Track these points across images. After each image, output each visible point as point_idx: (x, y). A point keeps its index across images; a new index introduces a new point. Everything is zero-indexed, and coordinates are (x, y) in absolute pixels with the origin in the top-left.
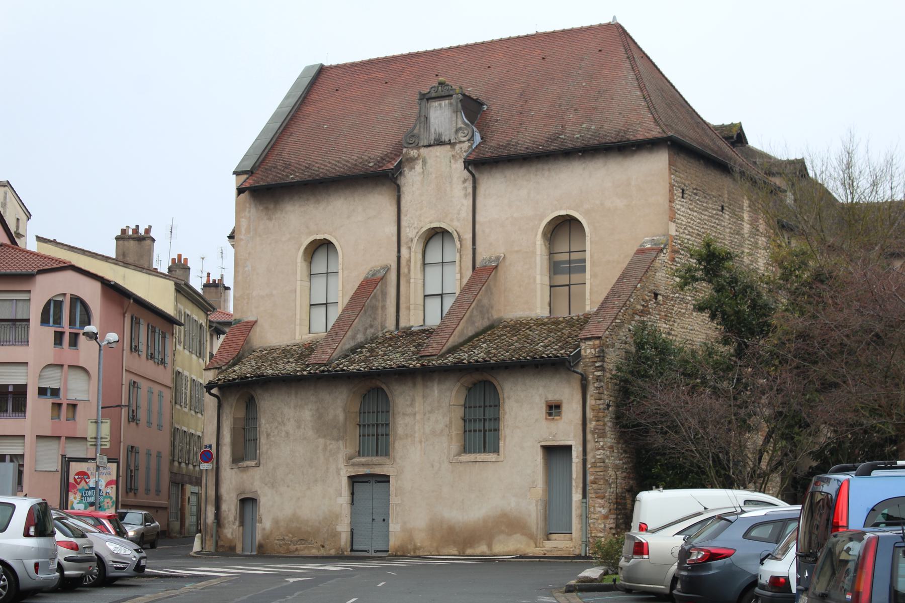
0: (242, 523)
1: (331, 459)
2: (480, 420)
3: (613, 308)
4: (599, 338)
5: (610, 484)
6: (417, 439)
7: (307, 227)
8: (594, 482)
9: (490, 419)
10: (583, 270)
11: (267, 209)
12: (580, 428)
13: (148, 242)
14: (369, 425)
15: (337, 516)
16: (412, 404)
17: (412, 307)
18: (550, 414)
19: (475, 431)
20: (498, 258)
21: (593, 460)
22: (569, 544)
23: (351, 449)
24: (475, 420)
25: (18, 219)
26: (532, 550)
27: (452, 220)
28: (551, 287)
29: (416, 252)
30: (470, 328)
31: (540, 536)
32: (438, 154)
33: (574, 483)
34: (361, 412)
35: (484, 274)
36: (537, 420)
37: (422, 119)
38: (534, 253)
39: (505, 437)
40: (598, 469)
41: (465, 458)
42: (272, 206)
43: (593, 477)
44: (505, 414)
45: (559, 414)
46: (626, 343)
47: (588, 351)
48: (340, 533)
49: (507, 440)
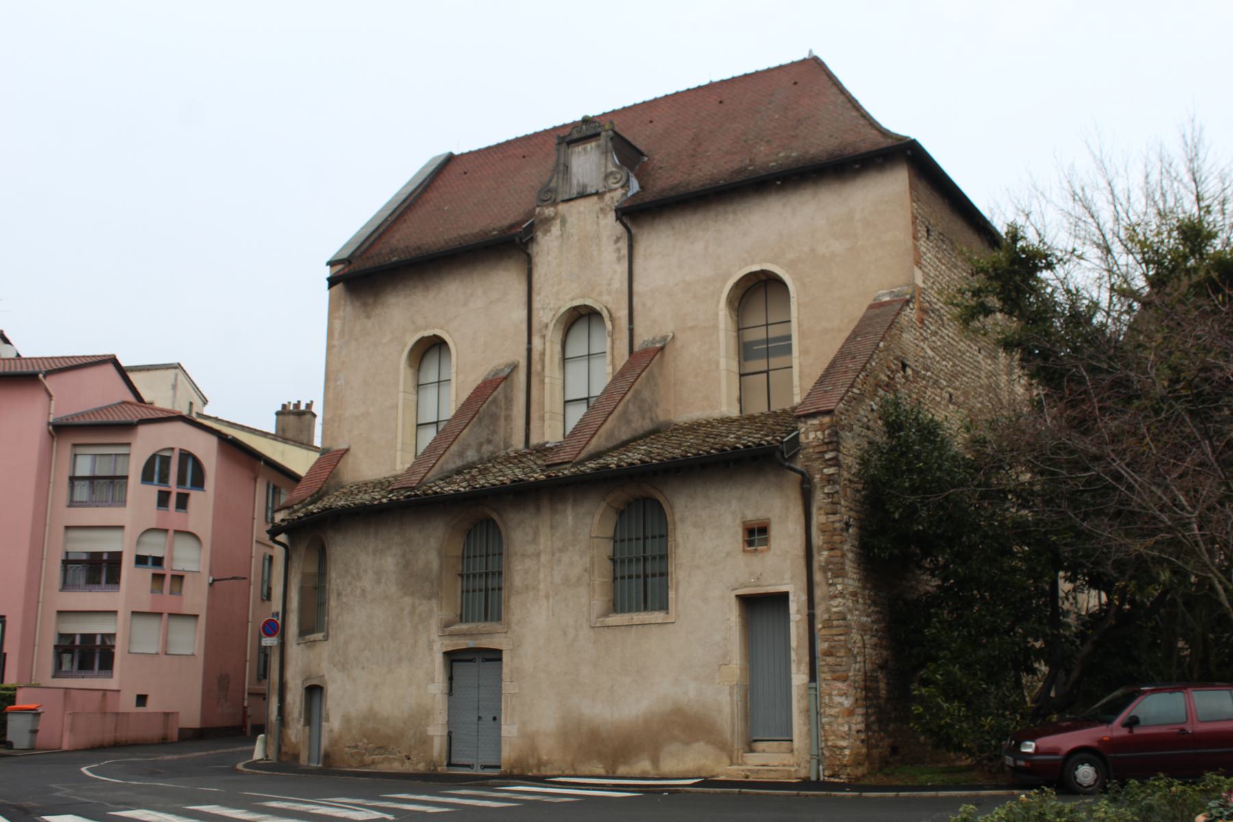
0: (308, 722)
1: (420, 627)
3: (846, 372)
4: (829, 412)
5: (855, 657)
6: (542, 593)
7: (414, 323)
9: (654, 558)
10: (788, 350)
11: (365, 305)
12: (802, 563)
13: (308, 417)
14: (474, 576)
15: (428, 713)
17: (547, 416)
18: (750, 543)
19: (630, 577)
20: (664, 338)
21: (826, 616)
22: (787, 759)
23: (448, 613)
24: (630, 561)
25: (191, 404)
26: (725, 770)
27: (600, 294)
28: (741, 375)
29: (552, 342)
30: (624, 429)
31: (738, 744)
32: (582, 209)
33: (793, 656)
34: (465, 557)
35: (645, 359)
36: (728, 554)
37: (561, 168)
38: (716, 327)
39: (677, 583)
40: (834, 631)
41: (615, 619)
42: (371, 301)
43: (826, 645)
44: (677, 546)
45: (766, 542)
46: (868, 428)
47: (812, 436)
48: (432, 738)
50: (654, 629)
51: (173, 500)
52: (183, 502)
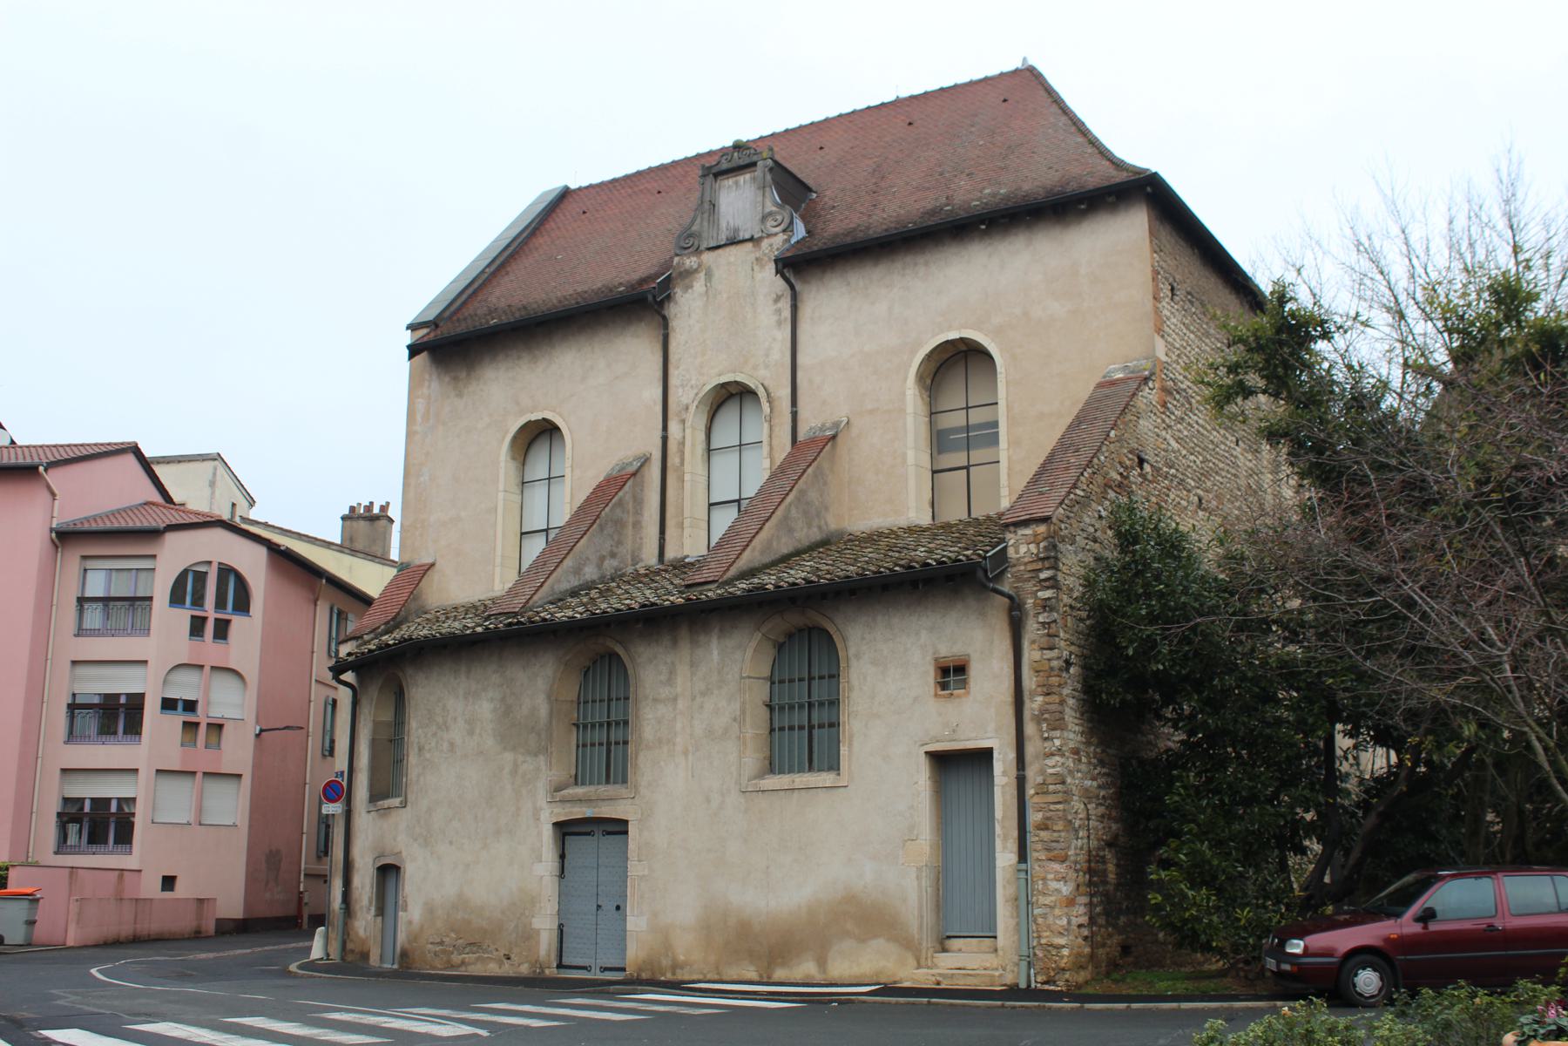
0: (381, 911)
2: (801, 706)
3: (1067, 469)
4: (1045, 520)
5: (1077, 831)
8: (1043, 826)
9: (821, 704)
10: (993, 440)
11: (456, 379)
12: (1009, 712)
13: (383, 522)
16: (669, 680)
17: (687, 523)
18: (944, 686)
19: (791, 728)
20: (836, 425)
21: (1040, 779)
22: (991, 960)
25: (234, 505)
26: (911, 975)
27: (755, 368)
28: (934, 472)
31: (927, 943)
34: (582, 702)
35: (811, 452)
37: (706, 206)
38: (902, 410)
39: (851, 737)
40: (1051, 798)
42: (463, 375)
43: (1040, 816)
44: (850, 690)
45: (964, 684)
47: (1023, 549)
48: (538, 932)
49: (856, 744)
50: (821, 794)
51: (210, 628)
52: (222, 630)
